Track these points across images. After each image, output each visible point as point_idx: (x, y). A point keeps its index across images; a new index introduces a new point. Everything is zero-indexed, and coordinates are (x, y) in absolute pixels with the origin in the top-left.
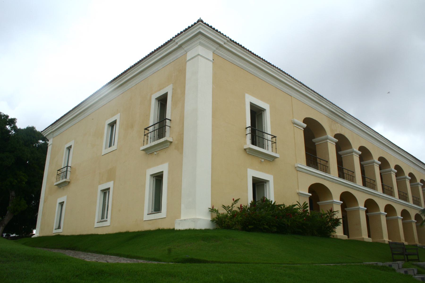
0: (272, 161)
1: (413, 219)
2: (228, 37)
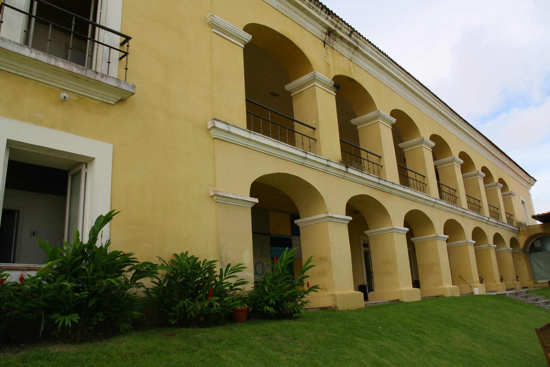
0: (113, 103)
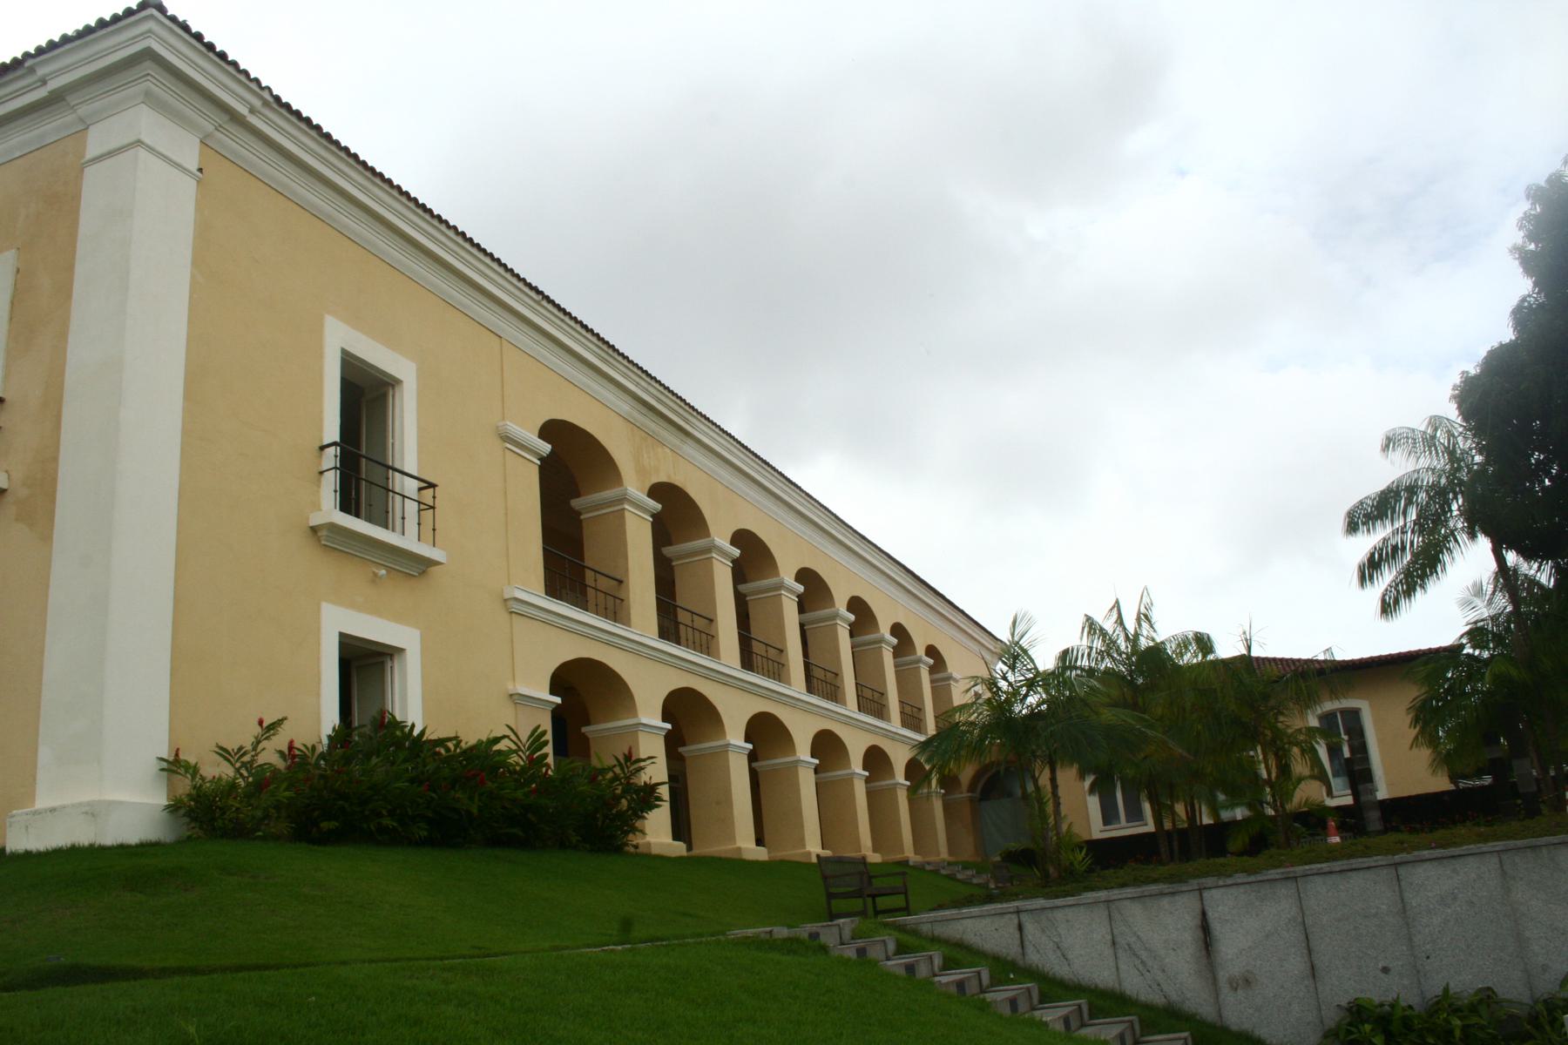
0: (415, 574)
1: (900, 777)
2: (269, 88)
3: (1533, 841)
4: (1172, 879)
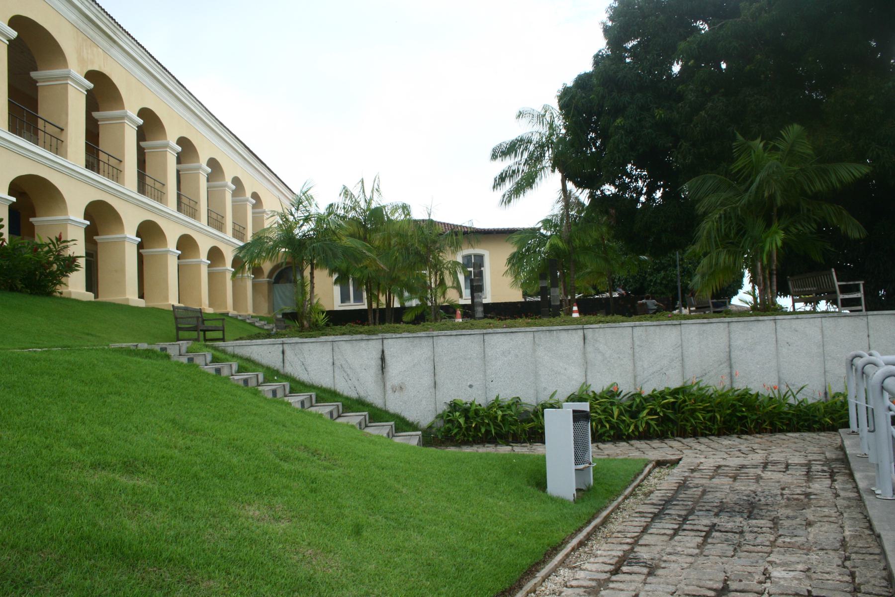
3: (551, 328)
4: (370, 333)
